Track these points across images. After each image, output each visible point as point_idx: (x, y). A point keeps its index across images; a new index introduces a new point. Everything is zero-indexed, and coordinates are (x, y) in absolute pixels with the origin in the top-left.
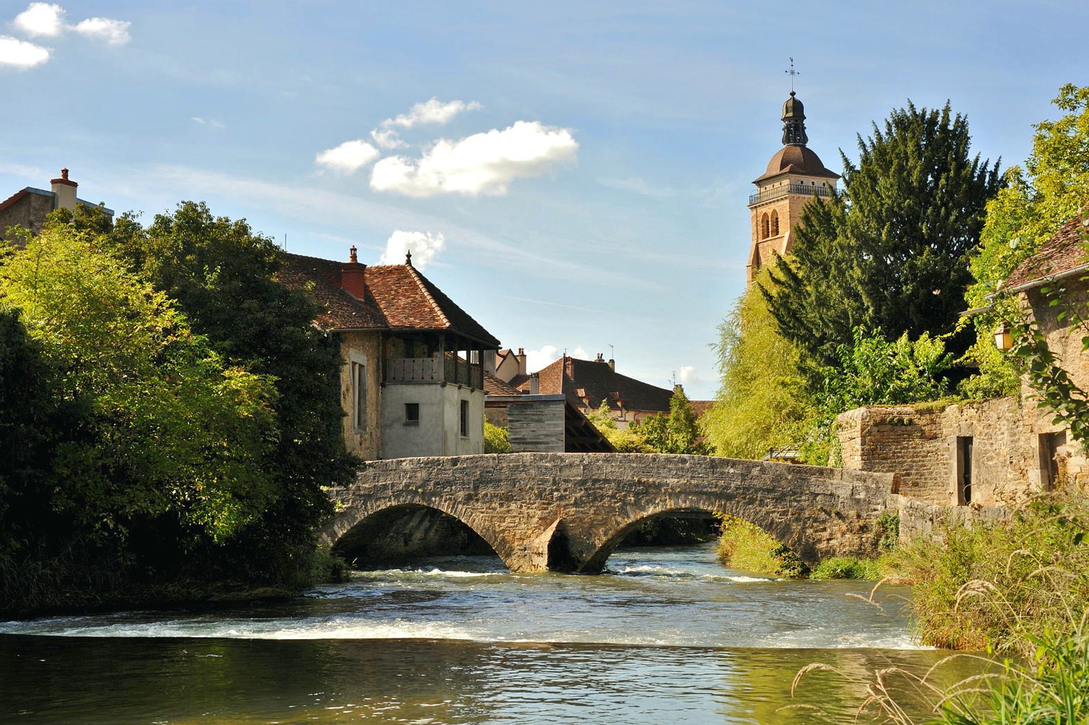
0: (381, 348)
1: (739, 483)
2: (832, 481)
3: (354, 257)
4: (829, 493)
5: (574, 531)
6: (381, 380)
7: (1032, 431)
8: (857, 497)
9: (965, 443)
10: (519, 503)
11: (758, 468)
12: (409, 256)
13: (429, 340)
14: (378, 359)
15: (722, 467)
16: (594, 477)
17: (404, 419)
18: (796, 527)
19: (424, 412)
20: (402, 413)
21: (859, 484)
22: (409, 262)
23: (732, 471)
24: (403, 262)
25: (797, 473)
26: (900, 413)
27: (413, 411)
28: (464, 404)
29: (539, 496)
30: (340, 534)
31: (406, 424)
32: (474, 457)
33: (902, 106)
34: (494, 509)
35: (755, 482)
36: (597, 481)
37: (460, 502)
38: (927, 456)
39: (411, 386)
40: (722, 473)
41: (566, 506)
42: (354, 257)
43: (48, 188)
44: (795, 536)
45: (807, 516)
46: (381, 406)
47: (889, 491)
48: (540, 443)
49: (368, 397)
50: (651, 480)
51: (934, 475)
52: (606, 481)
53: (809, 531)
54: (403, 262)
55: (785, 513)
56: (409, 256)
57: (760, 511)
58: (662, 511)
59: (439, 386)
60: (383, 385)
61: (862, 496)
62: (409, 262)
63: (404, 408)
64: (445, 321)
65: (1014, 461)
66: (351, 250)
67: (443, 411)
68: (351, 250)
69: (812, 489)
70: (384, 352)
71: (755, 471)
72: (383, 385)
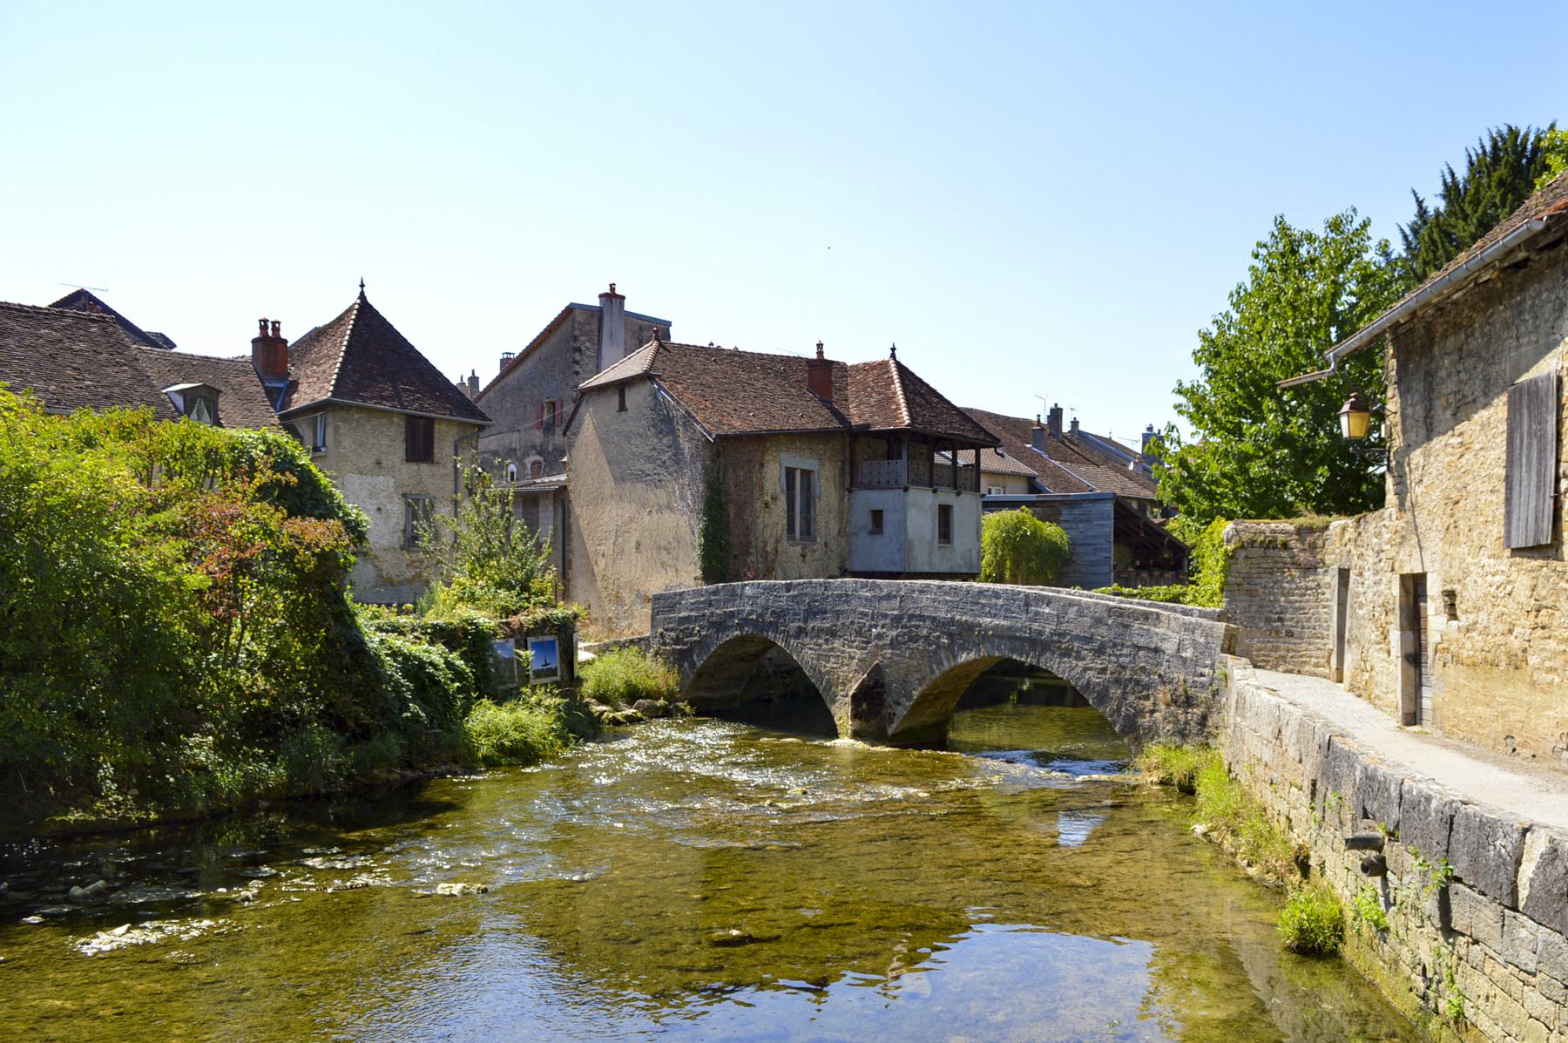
0: (848, 450)
1: (1054, 627)
2: (1157, 630)
3: (820, 353)
4: (1153, 646)
5: (891, 675)
6: (847, 484)
7: (1393, 570)
8: (1183, 655)
9: (1344, 575)
10: (842, 640)
11: (1076, 608)
12: (893, 349)
13: (893, 441)
14: (843, 463)
15: (1037, 605)
16: (910, 612)
17: (870, 527)
18: (1115, 692)
19: (888, 518)
20: (867, 520)
21: (1187, 636)
22: (893, 356)
23: (1047, 610)
24: (886, 356)
25: (1119, 617)
26: (1274, 531)
27: (877, 516)
28: (945, 512)
29: (859, 633)
30: (699, 664)
31: (872, 533)
32: (805, 583)
33: (1498, 122)
34: (820, 645)
35: (1071, 627)
36: (911, 617)
37: (792, 636)
38: (1304, 595)
39: (876, 491)
40: (1037, 613)
41: (882, 648)
42: (820, 353)
43: (596, 302)
44: (1114, 704)
45: (1128, 676)
46: (843, 515)
47: (1218, 649)
48: (1089, 545)
49: (820, 505)
50: (964, 618)
51: (1313, 622)
52: (921, 618)
53: (1131, 698)
54: (886, 356)
55: (1103, 671)
56: (893, 349)
57: (1077, 665)
58: (975, 660)
59: (901, 491)
60: (850, 491)
61: (1188, 654)
62: (893, 356)
63: (870, 515)
64: (906, 418)
65: (1376, 614)
66: (818, 345)
67: (905, 520)
68: (818, 345)
69: (1136, 639)
70: (852, 454)
71: (1072, 612)
72: (850, 491)
